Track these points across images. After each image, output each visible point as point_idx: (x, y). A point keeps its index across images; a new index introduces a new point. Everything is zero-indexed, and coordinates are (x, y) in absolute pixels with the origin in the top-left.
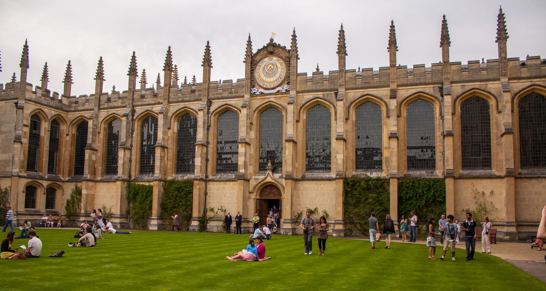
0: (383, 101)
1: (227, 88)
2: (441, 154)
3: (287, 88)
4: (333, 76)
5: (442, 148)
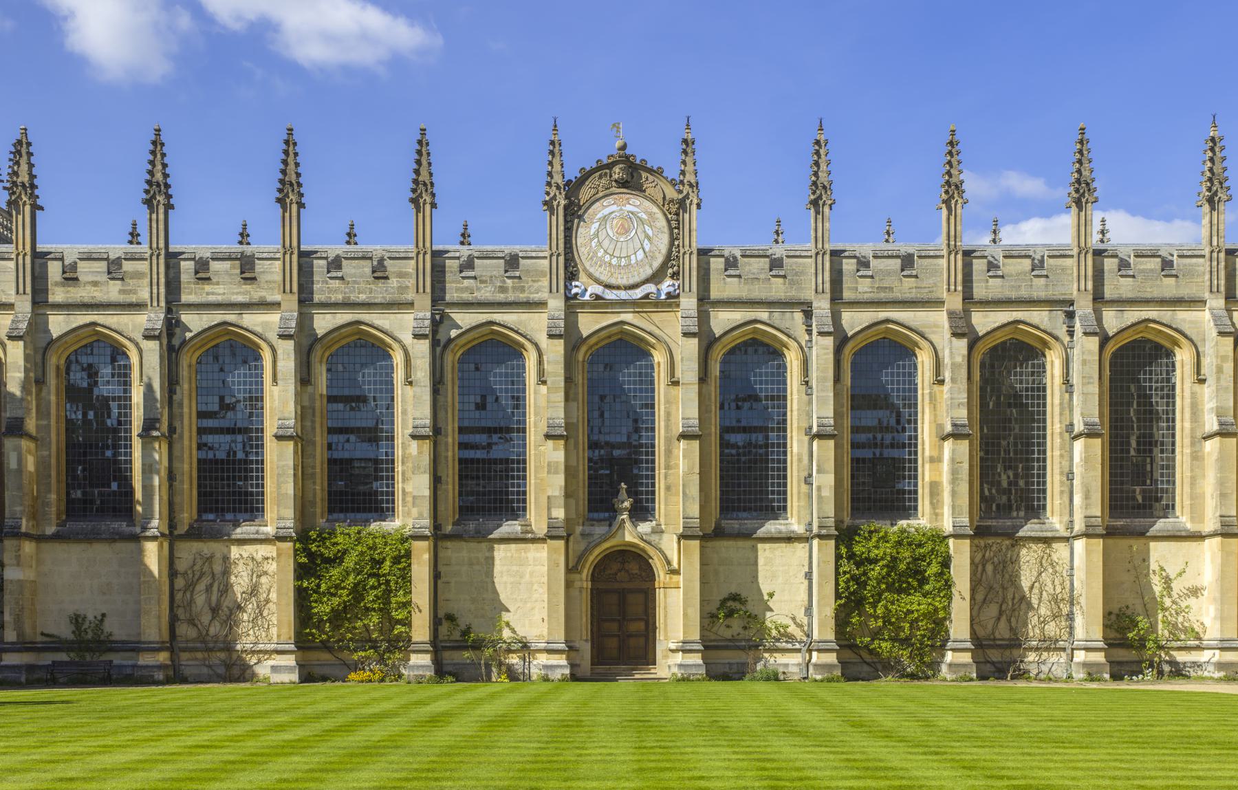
0: (926, 339)
1: (489, 274)
2: (1065, 479)
3: (671, 289)
4: (796, 263)
5: (1068, 463)
